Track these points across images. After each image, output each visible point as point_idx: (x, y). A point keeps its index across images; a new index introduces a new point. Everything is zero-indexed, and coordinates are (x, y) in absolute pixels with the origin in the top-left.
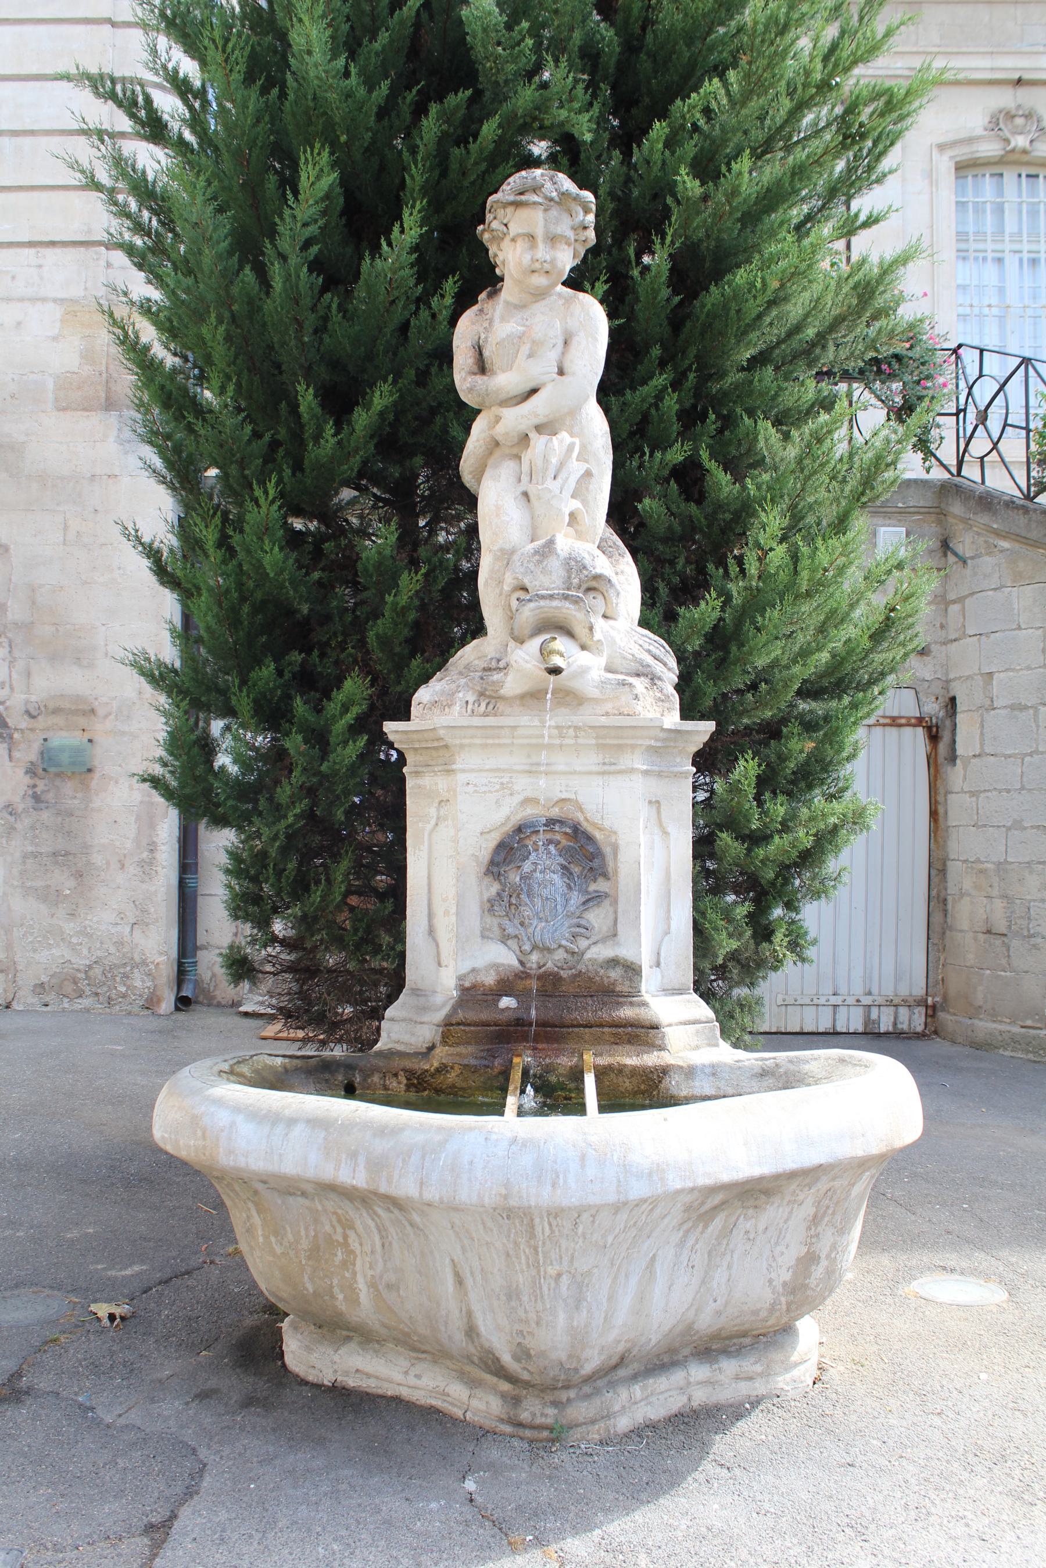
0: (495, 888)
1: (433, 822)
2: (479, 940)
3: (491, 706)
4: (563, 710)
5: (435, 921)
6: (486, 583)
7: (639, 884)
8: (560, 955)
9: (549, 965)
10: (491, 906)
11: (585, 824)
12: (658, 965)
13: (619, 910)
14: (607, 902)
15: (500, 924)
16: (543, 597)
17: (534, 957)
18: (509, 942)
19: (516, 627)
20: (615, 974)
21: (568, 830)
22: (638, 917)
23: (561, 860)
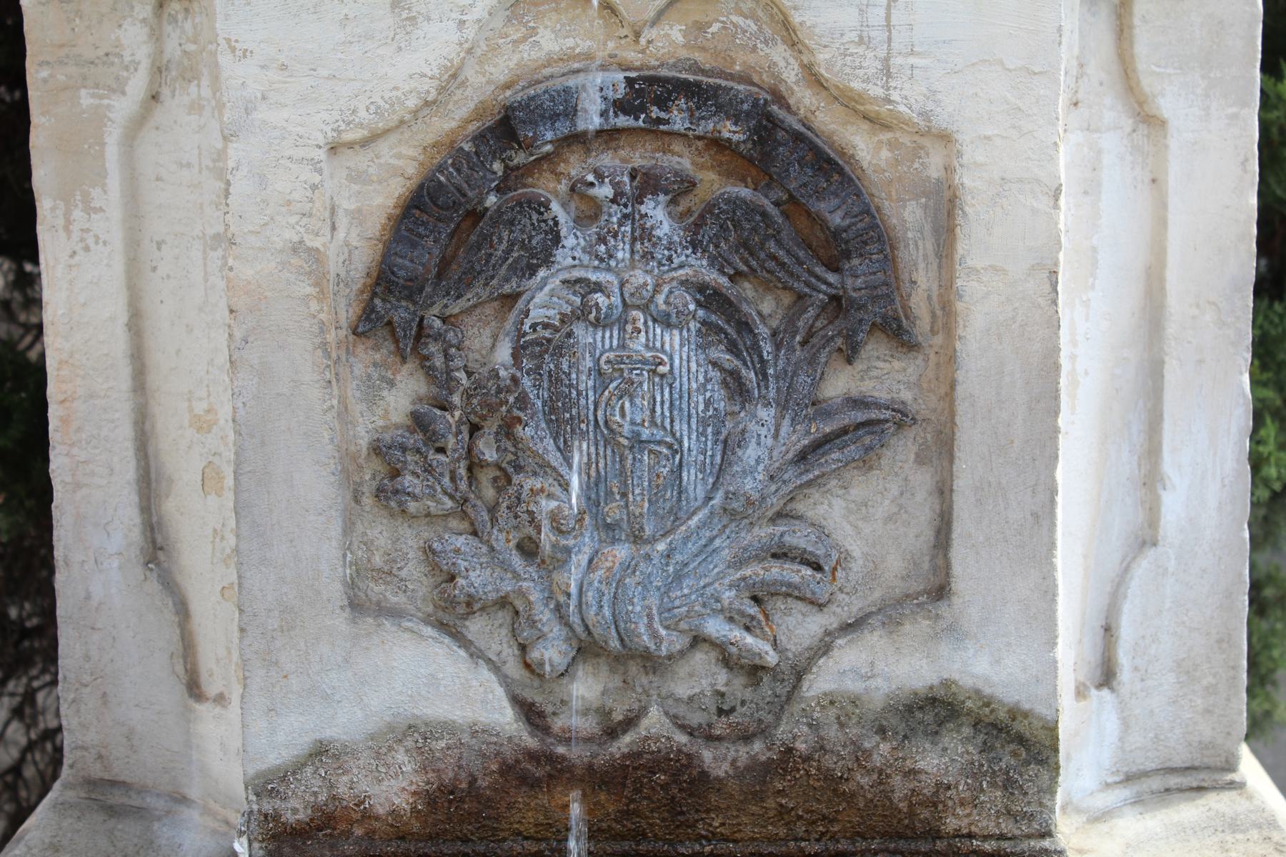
0: (403, 394)
1: (138, 85)
2: (340, 621)
5: (169, 506)
6: (1240, 713)
7: (1051, 368)
8: (699, 679)
9: (654, 722)
10: (387, 475)
11: (804, 98)
12: (1107, 676)
13: (963, 483)
14: (902, 450)
15: (429, 552)
17: (586, 688)
18: (475, 627)
20: (941, 759)
21: (729, 130)
22: (1044, 514)
23: (699, 268)
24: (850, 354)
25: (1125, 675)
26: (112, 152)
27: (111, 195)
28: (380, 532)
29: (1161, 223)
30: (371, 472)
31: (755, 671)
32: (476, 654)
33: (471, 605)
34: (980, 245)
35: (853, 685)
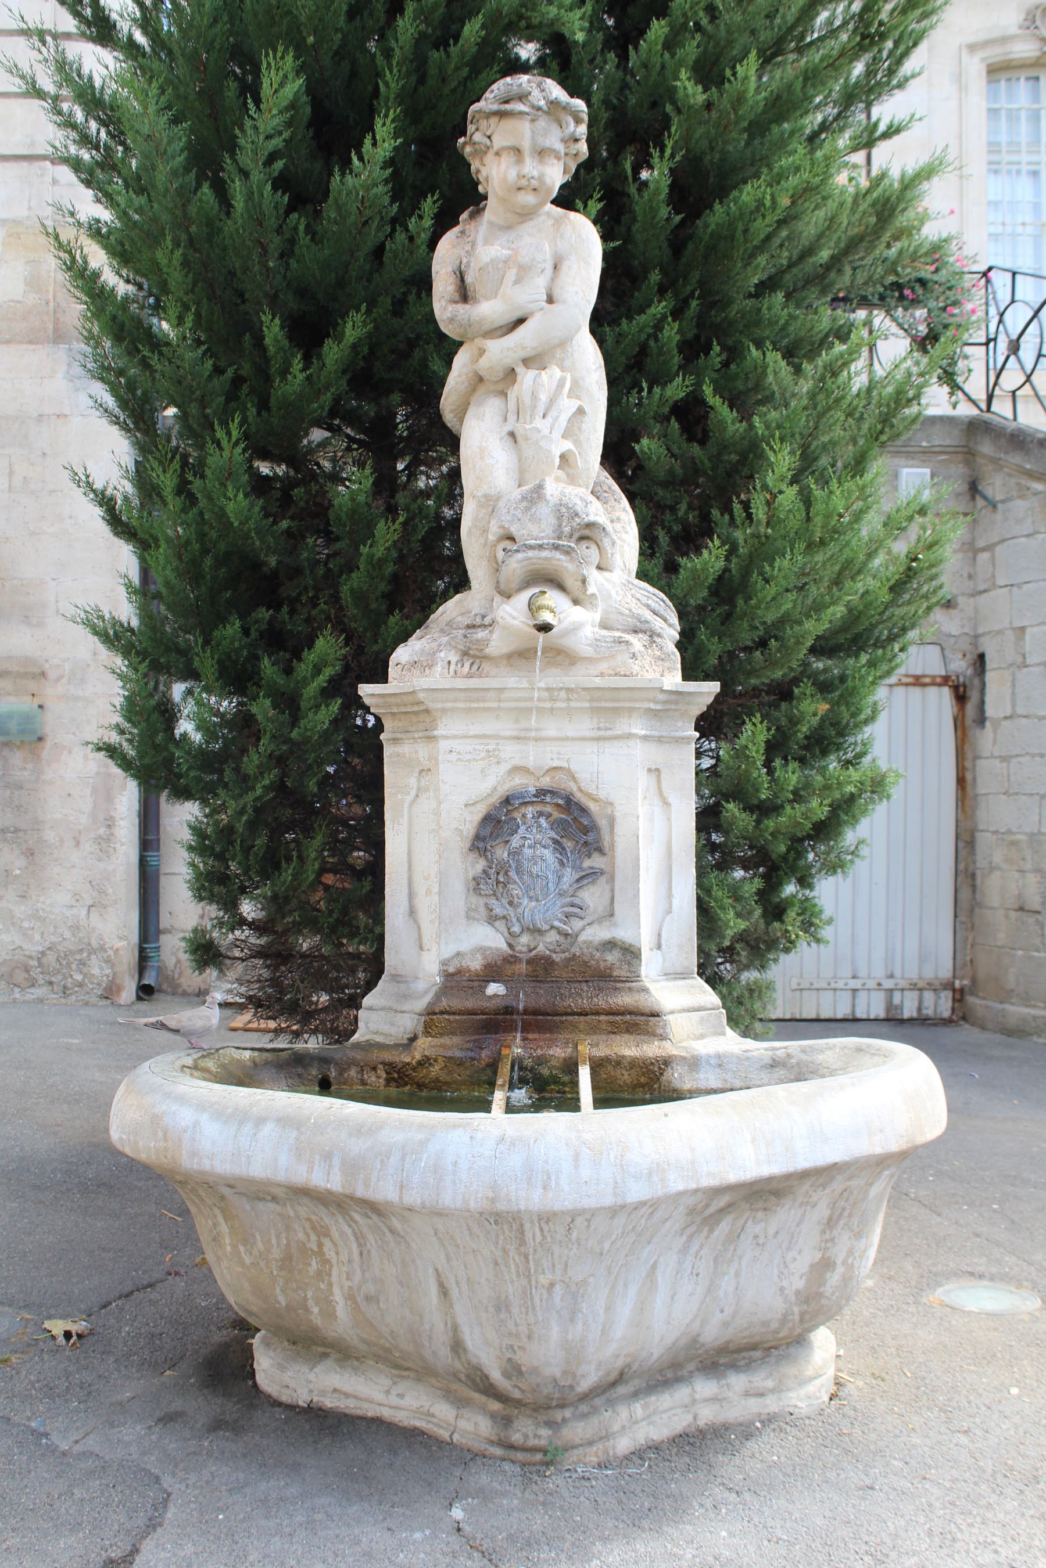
0: (481, 865)
1: (413, 793)
2: (464, 921)
3: (475, 667)
6: (470, 533)
8: (552, 937)
9: (541, 947)
10: (476, 885)
14: (602, 880)
15: (486, 905)
16: (531, 547)
17: (525, 939)
18: (497, 924)
20: (612, 957)
21: (560, 802)
24: (589, 856)
25: (664, 947)
26: (406, 810)
27: (405, 821)
28: (474, 899)
29: (670, 830)
30: (472, 884)
31: (566, 935)
32: (497, 930)
33: (496, 918)
34: (621, 830)
35: (590, 938)
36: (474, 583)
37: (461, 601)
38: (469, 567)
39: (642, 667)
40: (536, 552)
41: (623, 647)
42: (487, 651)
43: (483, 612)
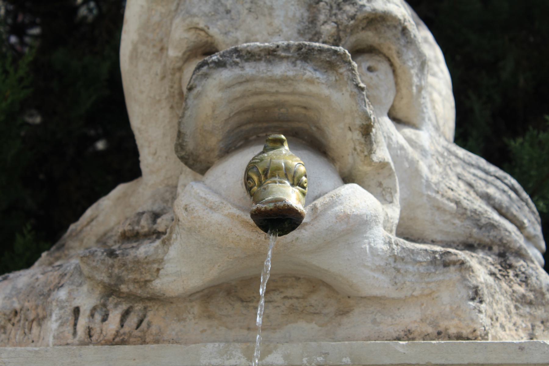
3: (132, 320)
4: (304, 327)
6: (134, 55)
16: (251, 56)
19: (188, 130)
36: (146, 159)
37: (125, 195)
38: (135, 123)
39: (494, 318)
40: (262, 66)
41: (453, 273)
42: (159, 285)
43: (156, 208)
